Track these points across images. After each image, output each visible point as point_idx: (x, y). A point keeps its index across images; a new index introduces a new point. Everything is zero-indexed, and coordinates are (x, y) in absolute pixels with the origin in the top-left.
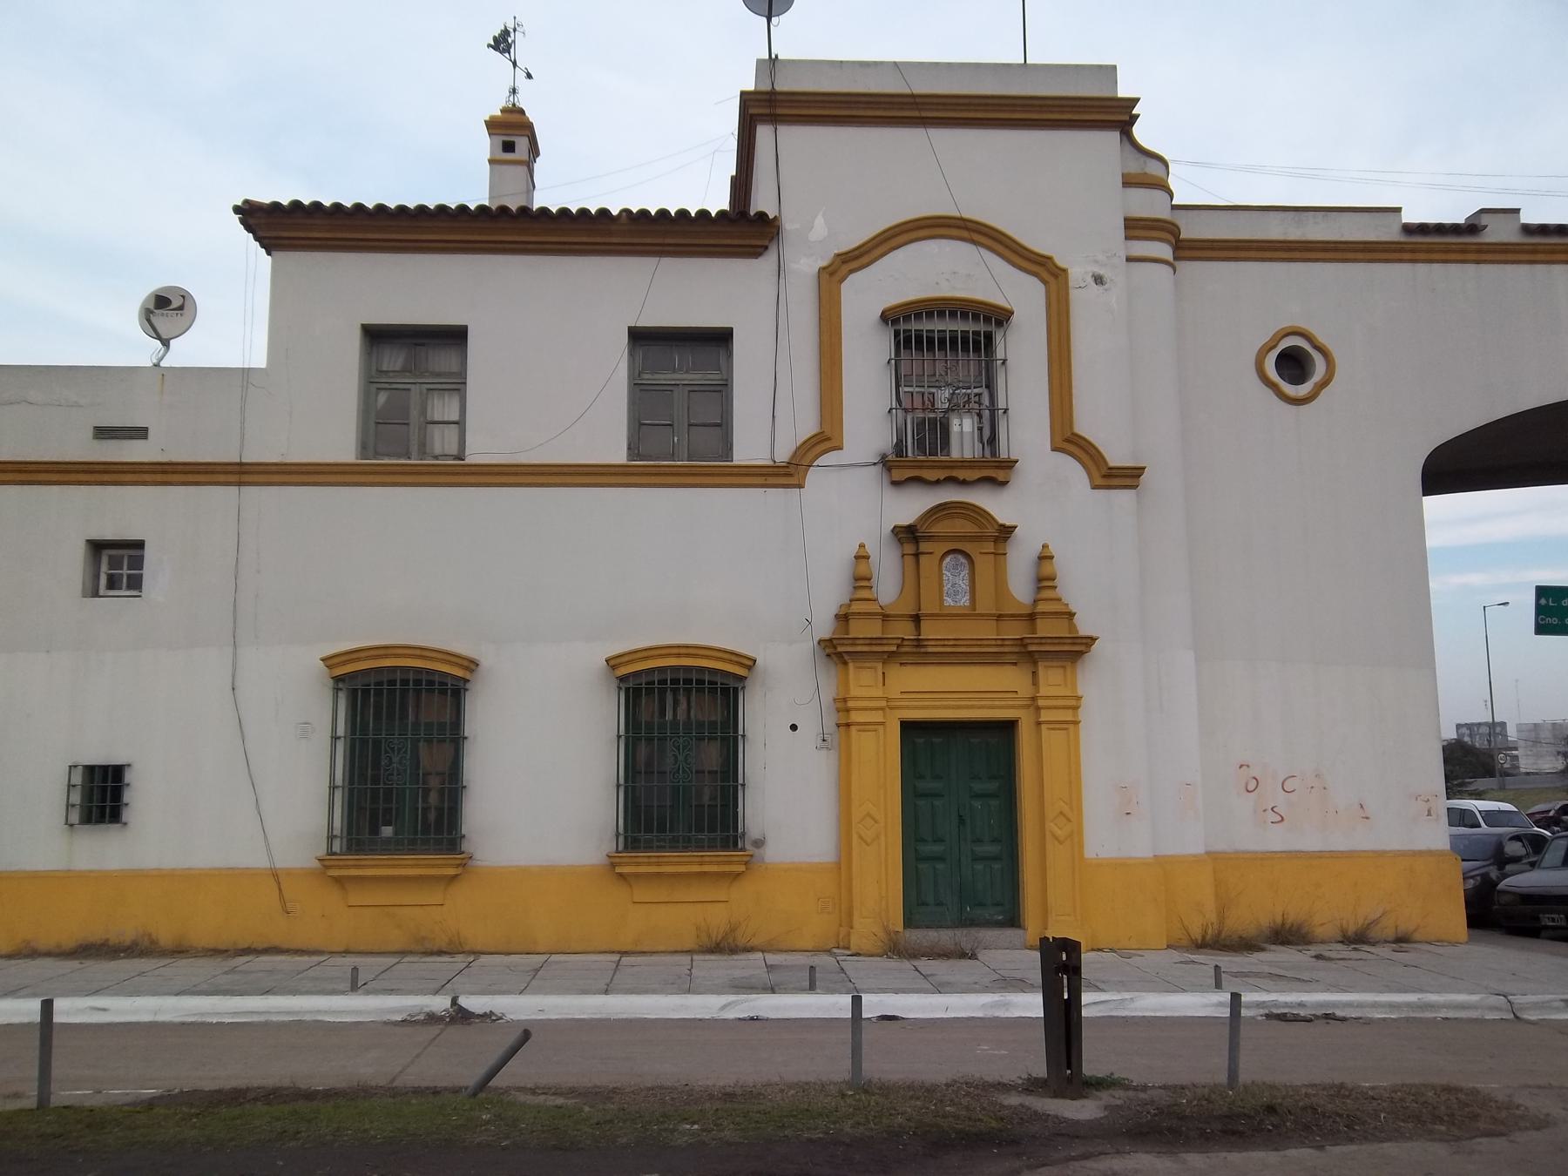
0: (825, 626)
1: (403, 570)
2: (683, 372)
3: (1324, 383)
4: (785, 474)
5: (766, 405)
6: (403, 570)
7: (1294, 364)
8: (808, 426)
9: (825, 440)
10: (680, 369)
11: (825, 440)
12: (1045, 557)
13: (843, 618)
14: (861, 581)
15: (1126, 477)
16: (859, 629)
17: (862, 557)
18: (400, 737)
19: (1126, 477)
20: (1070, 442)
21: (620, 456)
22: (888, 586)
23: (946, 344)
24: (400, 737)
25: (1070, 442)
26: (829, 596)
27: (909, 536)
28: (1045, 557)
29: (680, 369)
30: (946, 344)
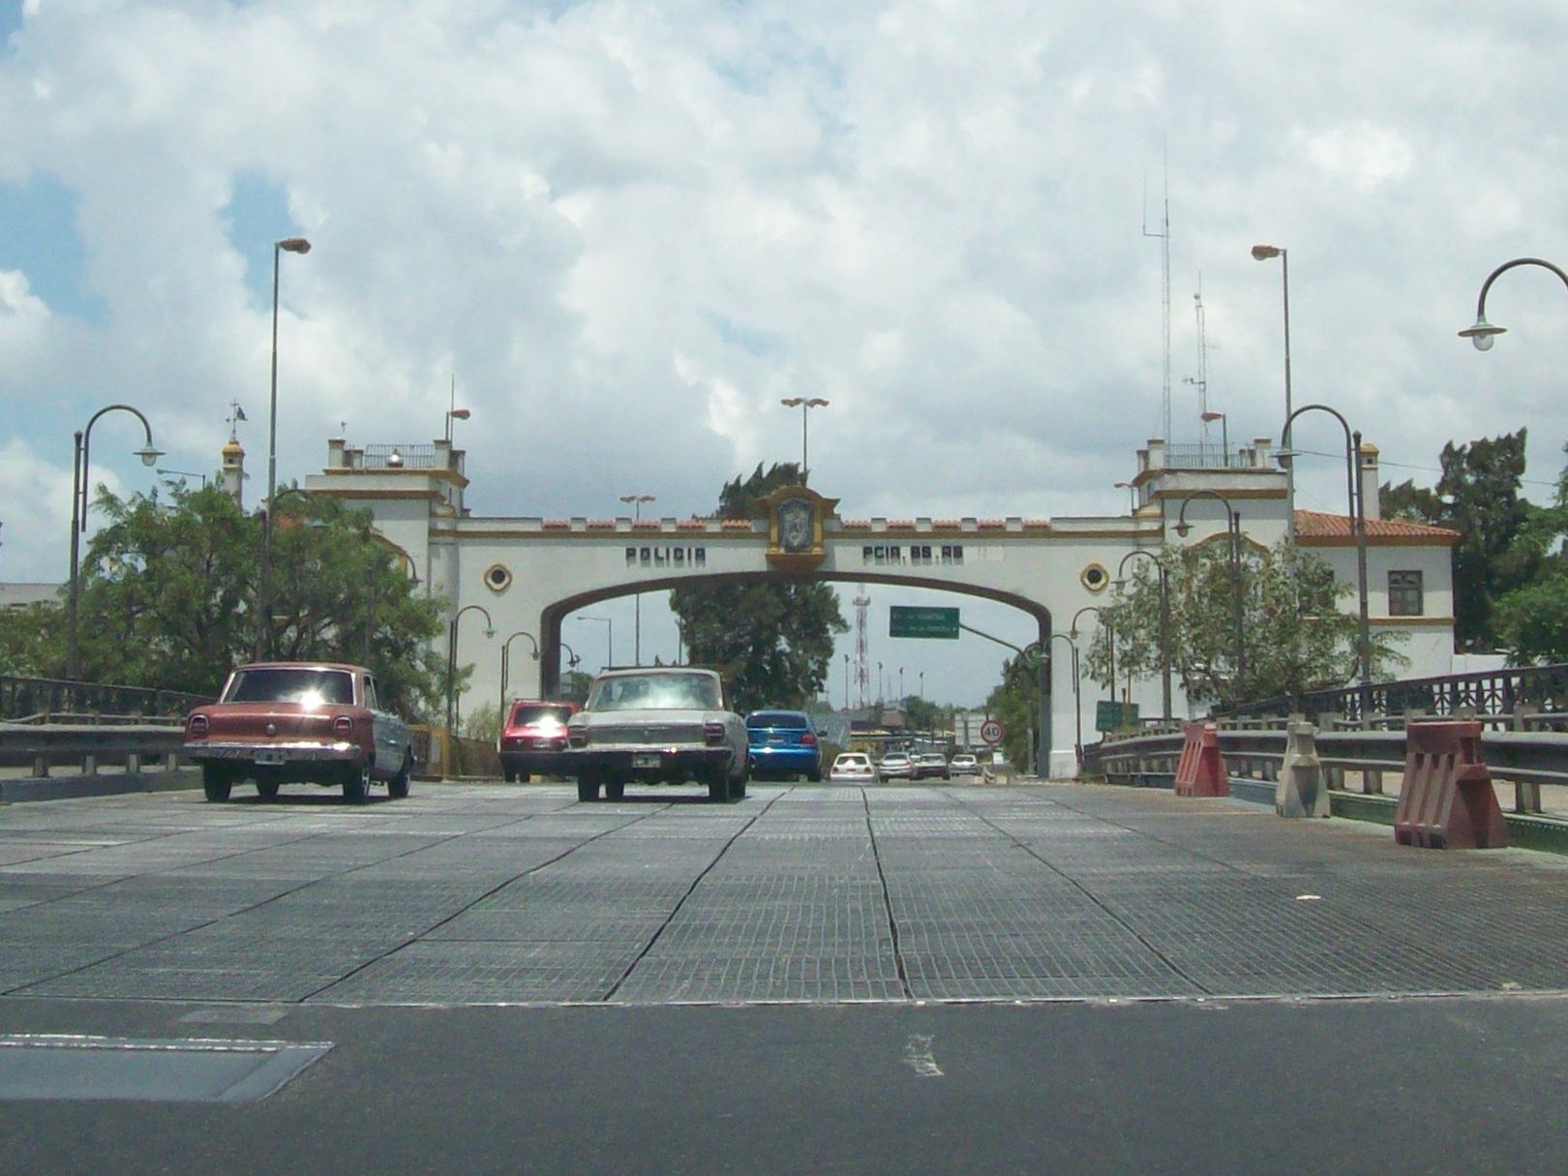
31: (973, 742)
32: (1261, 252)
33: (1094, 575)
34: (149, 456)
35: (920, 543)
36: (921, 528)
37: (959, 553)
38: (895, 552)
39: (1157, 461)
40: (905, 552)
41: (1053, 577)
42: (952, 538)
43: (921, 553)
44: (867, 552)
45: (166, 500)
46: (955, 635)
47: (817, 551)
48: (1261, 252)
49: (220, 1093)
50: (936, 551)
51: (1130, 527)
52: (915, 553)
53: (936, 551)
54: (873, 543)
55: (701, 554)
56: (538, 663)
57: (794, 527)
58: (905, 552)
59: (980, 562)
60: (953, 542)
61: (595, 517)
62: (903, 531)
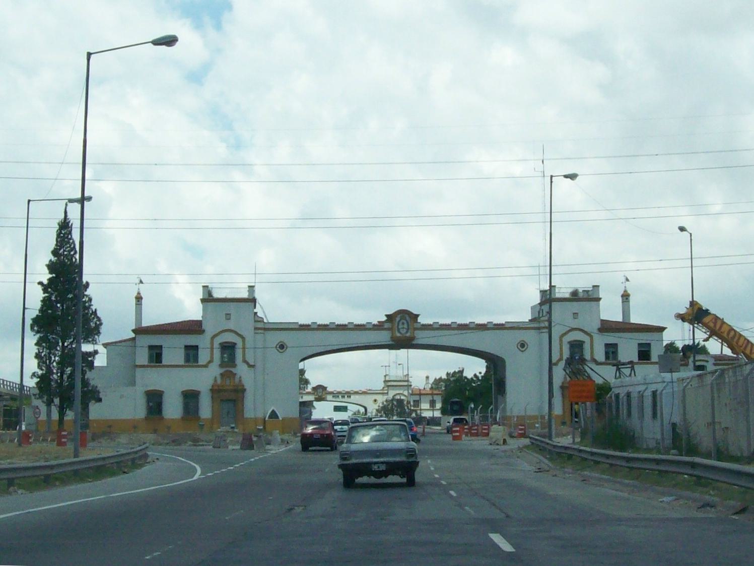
0: (561, 384)
1: (155, 379)
2: (192, 352)
3: (527, 348)
4: (206, 366)
5: (168, 357)
6: (155, 379)
7: (523, 345)
8: (209, 359)
9: (211, 361)
10: (192, 352)
11: (211, 361)
12: (240, 377)
13: (563, 383)
14: (215, 380)
15: (253, 366)
16: (565, 385)
17: (216, 378)
18: (155, 400)
19: (253, 366)
20: (245, 361)
21: (146, 363)
22: (219, 381)
23: (228, 349)
24: (155, 400)
25: (245, 361)
26: (211, 382)
27: (221, 374)
28: (240, 377)
29: (192, 352)
30: (228, 349)
31: (227, 384)
32: (682, 229)
33: (375, 401)
34: (136, 284)
35: (343, 395)
36: (335, 392)
37: (350, 397)
38: (338, 396)
39: (387, 379)
40: (340, 397)
41: (368, 401)
42: (349, 394)
43: (343, 397)
44: (333, 397)
45: (533, 486)
46: (346, 411)
47: (324, 397)
48: (682, 229)
49: (259, 304)
50: (346, 396)
51: (381, 392)
52: (342, 397)
53: (346, 396)
54: (334, 395)
55: (302, 397)
56: (85, 279)
57: (320, 392)
58: (340, 397)
59: (354, 398)
60: (349, 395)
61: (355, 390)
62: (339, 393)
